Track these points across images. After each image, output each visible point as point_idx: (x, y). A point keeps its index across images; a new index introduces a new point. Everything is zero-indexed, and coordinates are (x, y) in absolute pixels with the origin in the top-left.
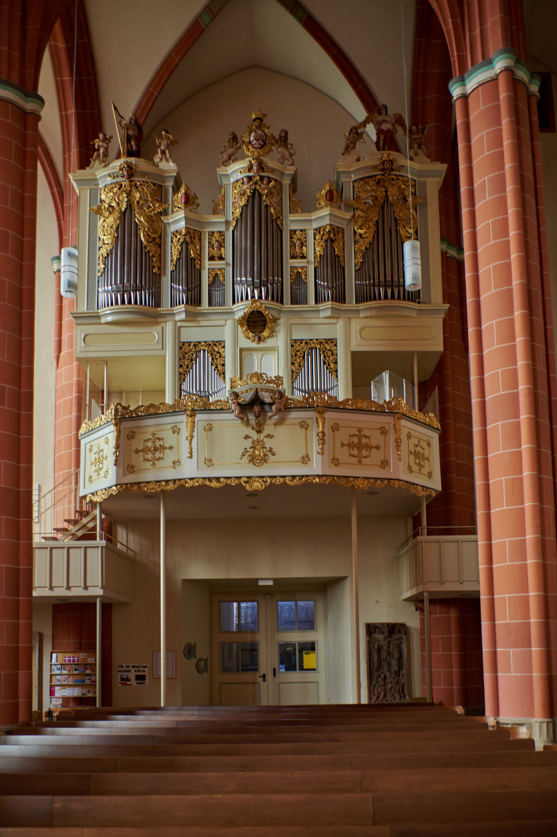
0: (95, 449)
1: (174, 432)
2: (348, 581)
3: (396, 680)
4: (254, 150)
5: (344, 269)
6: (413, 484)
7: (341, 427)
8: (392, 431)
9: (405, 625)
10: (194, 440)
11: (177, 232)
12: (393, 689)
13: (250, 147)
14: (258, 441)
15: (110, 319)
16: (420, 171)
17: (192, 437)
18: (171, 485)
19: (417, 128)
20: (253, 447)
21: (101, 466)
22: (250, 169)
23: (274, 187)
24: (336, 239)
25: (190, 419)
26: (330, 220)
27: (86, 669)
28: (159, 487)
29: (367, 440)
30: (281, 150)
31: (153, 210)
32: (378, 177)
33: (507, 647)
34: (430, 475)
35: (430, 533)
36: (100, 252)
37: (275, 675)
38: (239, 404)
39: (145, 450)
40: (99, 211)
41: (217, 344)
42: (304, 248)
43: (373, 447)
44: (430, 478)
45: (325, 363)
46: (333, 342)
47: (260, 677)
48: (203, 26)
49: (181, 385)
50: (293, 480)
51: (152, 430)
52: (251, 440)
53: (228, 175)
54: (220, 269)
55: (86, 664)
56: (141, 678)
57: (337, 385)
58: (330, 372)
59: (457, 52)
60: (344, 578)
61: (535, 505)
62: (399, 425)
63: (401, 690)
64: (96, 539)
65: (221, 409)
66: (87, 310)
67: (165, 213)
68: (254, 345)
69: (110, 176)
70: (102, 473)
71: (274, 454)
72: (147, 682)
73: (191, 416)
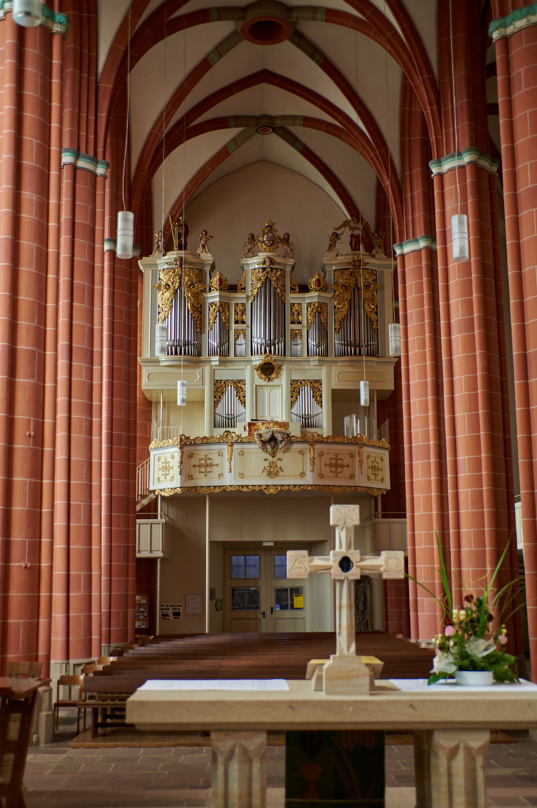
0: (163, 460)
1: (219, 455)
3: (362, 617)
4: (266, 247)
5: (327, 331)
6: (371, 488)
7: (325, 453)
9: (369, 576)
10: (233, 461)
11: (213, 303)
12: (360, 623)
13: (263, 244)
14: (273, 463)
15: (165, 364)
16: (379, 265)
18: (217, 490)
20: (270, 466)
21: (167, 472)
22: (264, 263)
23: (280, 275)
24: (322, 312)
25: (230, 448)
26: (318, 300)
27: (140, 607)
28: (209, 490)
29: (341, 462)
30: (285, 247)
31: (197, 289)
32: (351, 270)
33: (423, 597)
34: (382, 480)
35: (384, 516)
36: (159, 316)
37: (272, 613)
38: (262, 441)
39: (200, 466)
41: (240, 382)
43: (345, 466)
44: (382, 482)
45: (313, 397)
46: (319, 382)
47: (261, 614)
49: (215, 410)
50: (295, 488)
51: (205, 453)
52: (268, 462)
53: (248, 264)
54: (242, 330)
55: (140, 604)
56: (177, 615)
57: (322, 412)
58: (317, 403)
59: (398, 227)
61: (438, 513)
62: (362, 451)
63: (365, 624)
64: (158, 518)
65: (250, 442)
66: (150, 357)
68: (265, 383)
69: (167, 264)
70: (169, 477)
71: (282, 471)
72: (181, 617)
73: (230, 446)
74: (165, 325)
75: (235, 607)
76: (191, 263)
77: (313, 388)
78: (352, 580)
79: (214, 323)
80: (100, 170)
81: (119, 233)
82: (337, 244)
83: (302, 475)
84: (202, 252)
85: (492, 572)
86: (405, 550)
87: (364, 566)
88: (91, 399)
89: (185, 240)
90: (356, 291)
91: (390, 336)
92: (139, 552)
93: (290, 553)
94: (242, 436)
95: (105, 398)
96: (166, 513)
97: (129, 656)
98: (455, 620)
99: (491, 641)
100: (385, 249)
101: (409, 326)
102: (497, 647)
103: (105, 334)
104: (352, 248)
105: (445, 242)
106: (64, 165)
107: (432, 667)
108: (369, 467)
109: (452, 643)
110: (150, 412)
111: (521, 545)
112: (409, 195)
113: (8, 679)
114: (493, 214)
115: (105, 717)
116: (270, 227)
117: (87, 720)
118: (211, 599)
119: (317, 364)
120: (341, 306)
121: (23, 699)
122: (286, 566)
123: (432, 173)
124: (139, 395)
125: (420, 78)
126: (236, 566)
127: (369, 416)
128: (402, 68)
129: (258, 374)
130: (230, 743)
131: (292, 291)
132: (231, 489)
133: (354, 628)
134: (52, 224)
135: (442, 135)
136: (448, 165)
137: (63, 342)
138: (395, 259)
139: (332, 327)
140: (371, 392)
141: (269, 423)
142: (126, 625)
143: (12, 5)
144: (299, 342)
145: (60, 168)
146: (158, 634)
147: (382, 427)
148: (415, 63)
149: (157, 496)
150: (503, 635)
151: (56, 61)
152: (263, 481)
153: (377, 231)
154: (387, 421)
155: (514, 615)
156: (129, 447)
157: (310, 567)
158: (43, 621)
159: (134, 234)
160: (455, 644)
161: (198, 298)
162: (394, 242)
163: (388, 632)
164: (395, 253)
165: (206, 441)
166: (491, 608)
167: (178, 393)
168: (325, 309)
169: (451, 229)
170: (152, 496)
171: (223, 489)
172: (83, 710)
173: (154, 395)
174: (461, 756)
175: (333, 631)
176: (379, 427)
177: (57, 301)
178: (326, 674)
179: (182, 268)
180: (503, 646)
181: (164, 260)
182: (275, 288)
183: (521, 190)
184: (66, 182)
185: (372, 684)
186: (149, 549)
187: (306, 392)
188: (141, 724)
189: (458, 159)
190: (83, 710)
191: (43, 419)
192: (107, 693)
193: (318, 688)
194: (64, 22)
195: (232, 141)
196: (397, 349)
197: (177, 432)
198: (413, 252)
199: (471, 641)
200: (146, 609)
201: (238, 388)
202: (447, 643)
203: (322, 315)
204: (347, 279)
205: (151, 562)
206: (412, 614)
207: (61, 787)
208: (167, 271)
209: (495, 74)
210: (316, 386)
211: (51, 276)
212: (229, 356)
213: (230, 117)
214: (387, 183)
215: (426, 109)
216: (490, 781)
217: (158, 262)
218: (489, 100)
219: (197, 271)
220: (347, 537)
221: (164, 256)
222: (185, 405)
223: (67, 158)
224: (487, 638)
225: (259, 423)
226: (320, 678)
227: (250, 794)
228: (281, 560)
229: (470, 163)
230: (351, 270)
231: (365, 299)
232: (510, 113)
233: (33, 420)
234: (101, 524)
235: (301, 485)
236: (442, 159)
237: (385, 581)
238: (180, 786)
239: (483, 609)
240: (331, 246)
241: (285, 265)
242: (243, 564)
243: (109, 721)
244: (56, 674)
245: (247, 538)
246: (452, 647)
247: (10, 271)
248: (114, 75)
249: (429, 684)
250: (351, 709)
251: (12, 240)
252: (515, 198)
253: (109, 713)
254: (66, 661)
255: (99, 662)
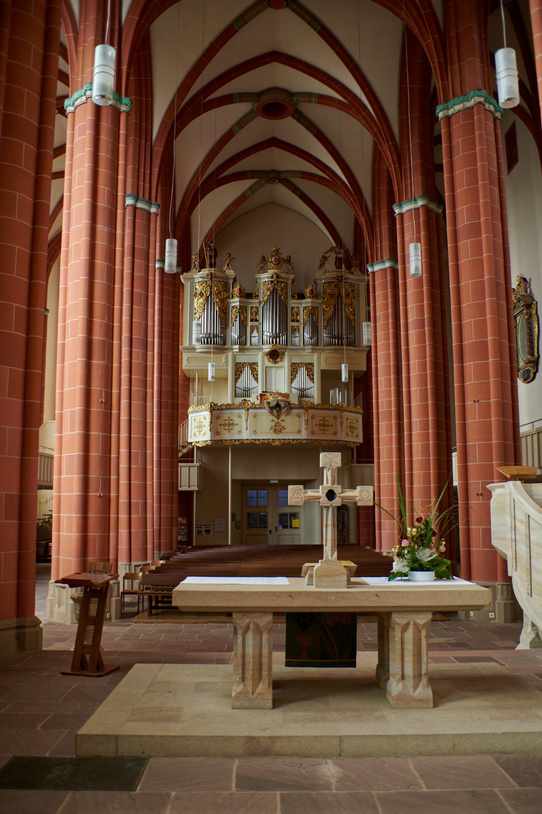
0: (197, 421)
2: (317, 481)
8: (339, 418)
10: (248, 421)
11: (235, 306)
13: (272, 264)
14: (278, 423)
15: (199, 351)
17: (247, 420)
19: (356, 257)
20: (276, 426)
22: (272, 277)
23: (284, 286)
27: (181, 526)
29: (327, 422)
30: (287, 265)
32: (335, 283)
34: (357, 436)
35: (358, 462)
37: (276, 531)
38: (270, 407)
39: (225, 425)
40: (195, 295)
42: (298, 316)
45: (307, 375)
46: (312, 364)
48: (248, 196)
49: (236, 384)
51: (228, 415)
52: (274, 422)
53: (260, 278)
60: (316, 480)
65: (261, 408)
67: (228, 297)
68: (273, 365)
70: (202, 433)
71: (285, 429)
72: (211, 533)
74: (199, 322)
75: (250, 527)
76: (218, 277)
77: (307, 369)
78: (335, 506)
79: (235, 321)
80: (153, 210)
81: (167, 254)
82: (325, 264)
83: (299, 432)
84: (227, 269)
85: (436, 502)
86: (374, 486)
87: (344, 496)
88: (145, 375)
89: (215, 261)
90: (339, 299)
91: (364, 331)
92: (181, 486)
93: (290, 487)
94: (255, 404)
95: (156, 375)
96: (200, 459)
97: (174, 560)
98: (409, 535)
99: (434, 550)
100: (361, 268)
101: (377, 324)
102: (438, 554)
103: (156, 328)
104: (336, 267)
105: (404, 263)
106: (128, 206)
107: (392, 568)
108: (348, 427)
109: (406, 552)
110: (189, 386)
111: (456, 483)
112: (378, 229)
113: (88, 574)
114: (439, 244)
115: (157, 602)
116: (277, 251)
117: (144, 604)
118: (232, 521)
119: (310, 351)
120: (328, 309)
121: (99, 589)
122: (287, 497)
123: (395, 213)
124: (181, 373)
125: (431, 37)
126: (251, 497)
127: (348, 390)
128: (373, 138)
129: (268, 359)
130: (247, 621)
131: (293, 298)
132: (247, 442)
133: (336, 541)
134: (118, 248)
135: (402, 186)
136: (406, 208)
137: (125, 335)
138: (368, 275)
139: (322, 324)
140: (350, 372)
141: (275, 394)
142: (172, 539)
143: (92, 93)
144: (297, 335)
145: (124, 208)
146: (194, 545)
147: (357, 397)
148: (383, 134)
149: (194, 446)
150: (443, 545)
151: (122, 132)
152: (271, 436)
153: (355, 255)
154: (361, 394)
155: (450, 532)
156: (173, 411)
157: (305, 496)
158: (112, 534)
159: (177, 255)
160: (409, 552)
161: (223, 302)
162: (367, 263)
163: (359, 545)
164: (368, 271)
165: (229, 407)
166: (433, 526)
167: (209, 371)
168: (316, 312)
169: (409, 253)
170: (190, 446)
171: (241, 442)
172: (141, 597)
173: (192, 373)
174: (411, 630)
175: (320, 544)
176: (355, 397)
177: (121, 304)
178: (316, 573)
179: (212, 281)
180: (442, 553)
181: (199, 275)
182: (280, 295)
183: (459, 226)
184: (128, 218)
185: (348, 580)
186: (188, 485)
187: (302, 372)
188: (183, 607)
189: (414, 203)
190: (141, 597)
191: (112, 390)
192: (158, 586)
193: (310, 583)
194: (128, 104)
195: (249, 188)
196: (369, 341)
197: (208, 400)
198: (381, 270)
199: (420, 550)
200: (185, 527)
201: (253, 369)
202: (403, 551)
203: (314, 315)
204: (332, 289)
205: (189, 494)
206: (377, 532)
207: (127, 649)
208: (201, 283)
209: (441, 143)
210: (309, 367)
211: (117, 286)
212: (246, 345)
213: (247, 171)
214: (362, 220)
215: (391, 167)
216: (430, 647)
217: (195, 276)
218: (437, 162)
219: (223, 283)
220: (332, 476)
221: (199, 272)
222: (214, 380)
223: (129, 201)
224: (430, 548)
225: (268, 394)
226: (311, 576)
227: (261, 655)
228: (283, 493)
229: (422, 206)
230: (335, 283)
231: (346, 304)
232: (452, 171)
233: (105, 391)
234: (153, 466)
235: (298, 439)
236: (402, 203)
237: (358, 508)
238: (211, 650)
239: (429, 527)
240: (321, 265)
241: (288, 279)
242: (256, 496)
243: (160, 605)
244: (122, 571)
245: (259, 477)
246: (406, 554)
247: (88, 281)
248: (164, 141)
249: (389, 580)
250: (333, 598)
251: (90, 260)
252: (455, 232)
253: (160, 599)
254: (129, 563)
255: (153, 564)
